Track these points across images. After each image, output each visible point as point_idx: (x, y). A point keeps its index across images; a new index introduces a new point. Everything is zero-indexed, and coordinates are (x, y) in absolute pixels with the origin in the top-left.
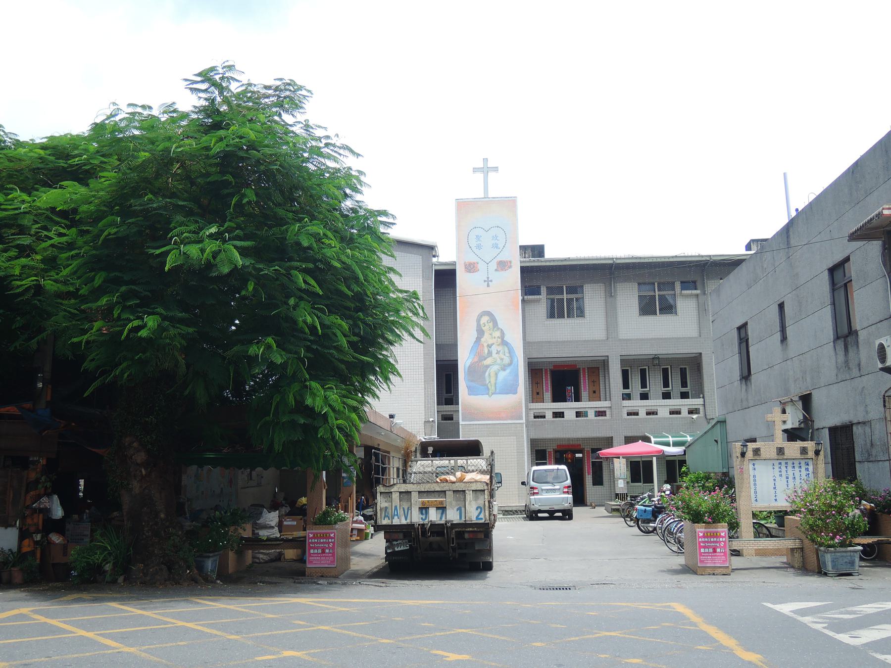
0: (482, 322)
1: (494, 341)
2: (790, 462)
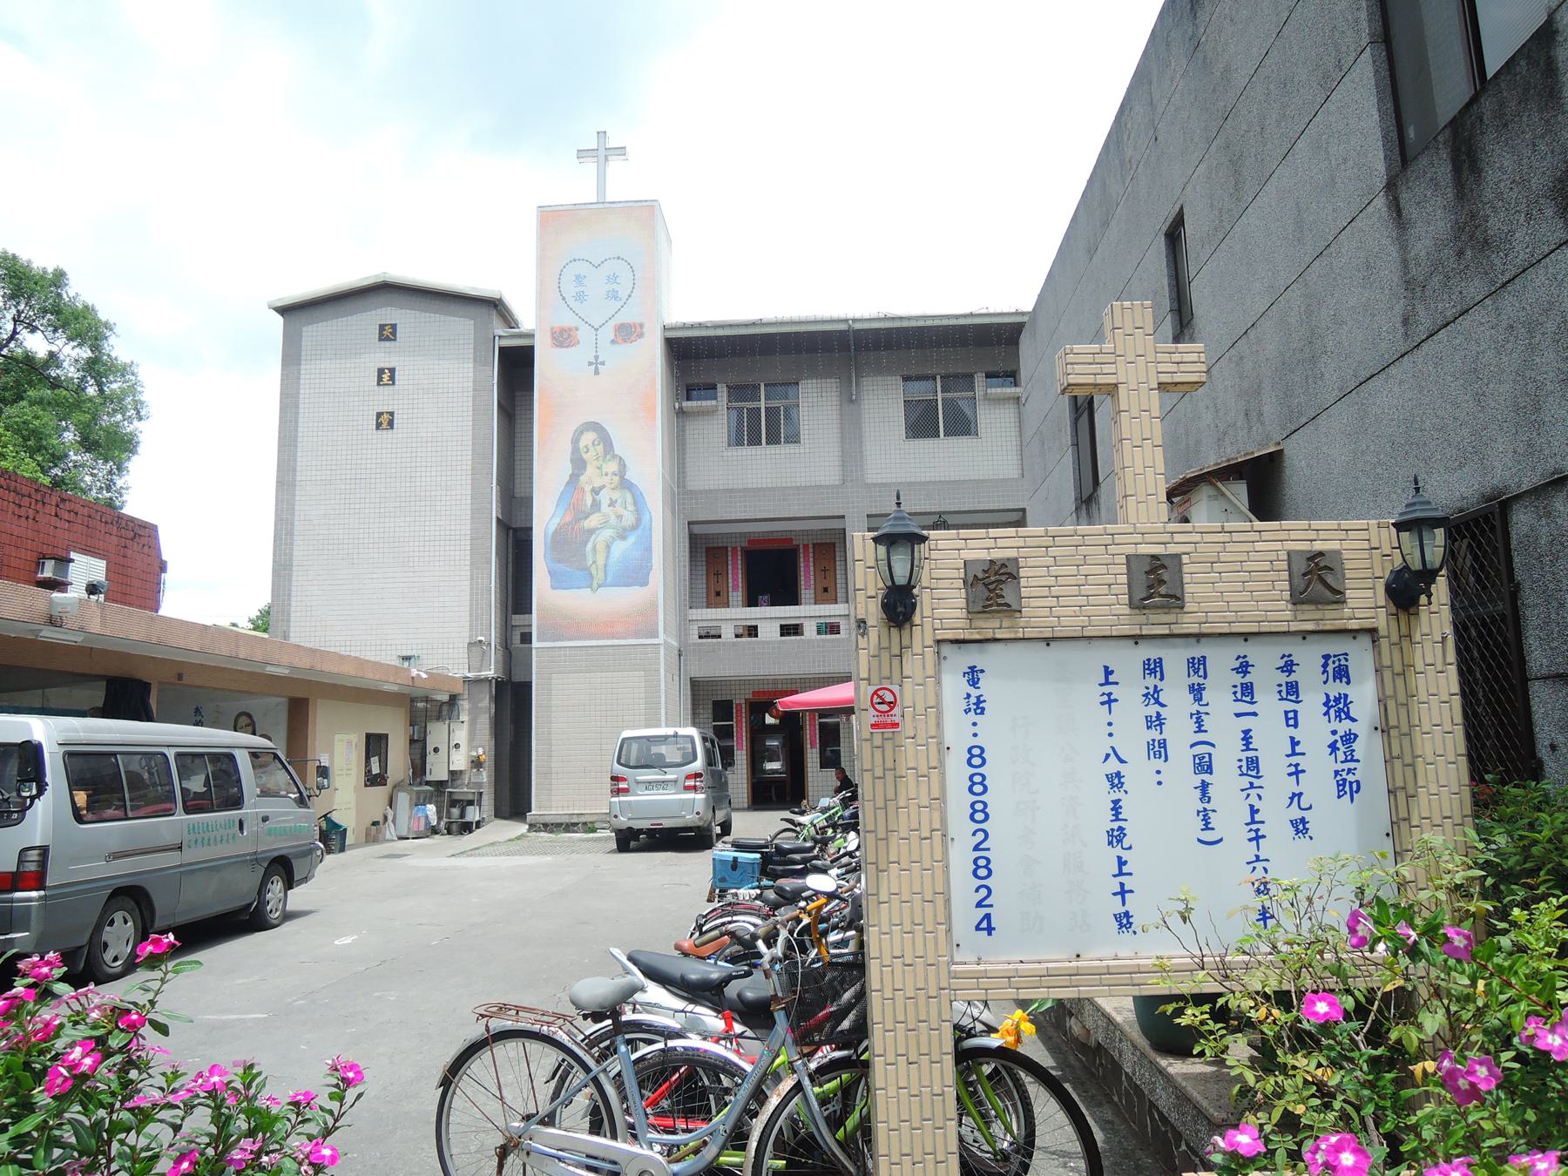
0: (582, 445)
1: (606, 480)
2: (1221, 660)
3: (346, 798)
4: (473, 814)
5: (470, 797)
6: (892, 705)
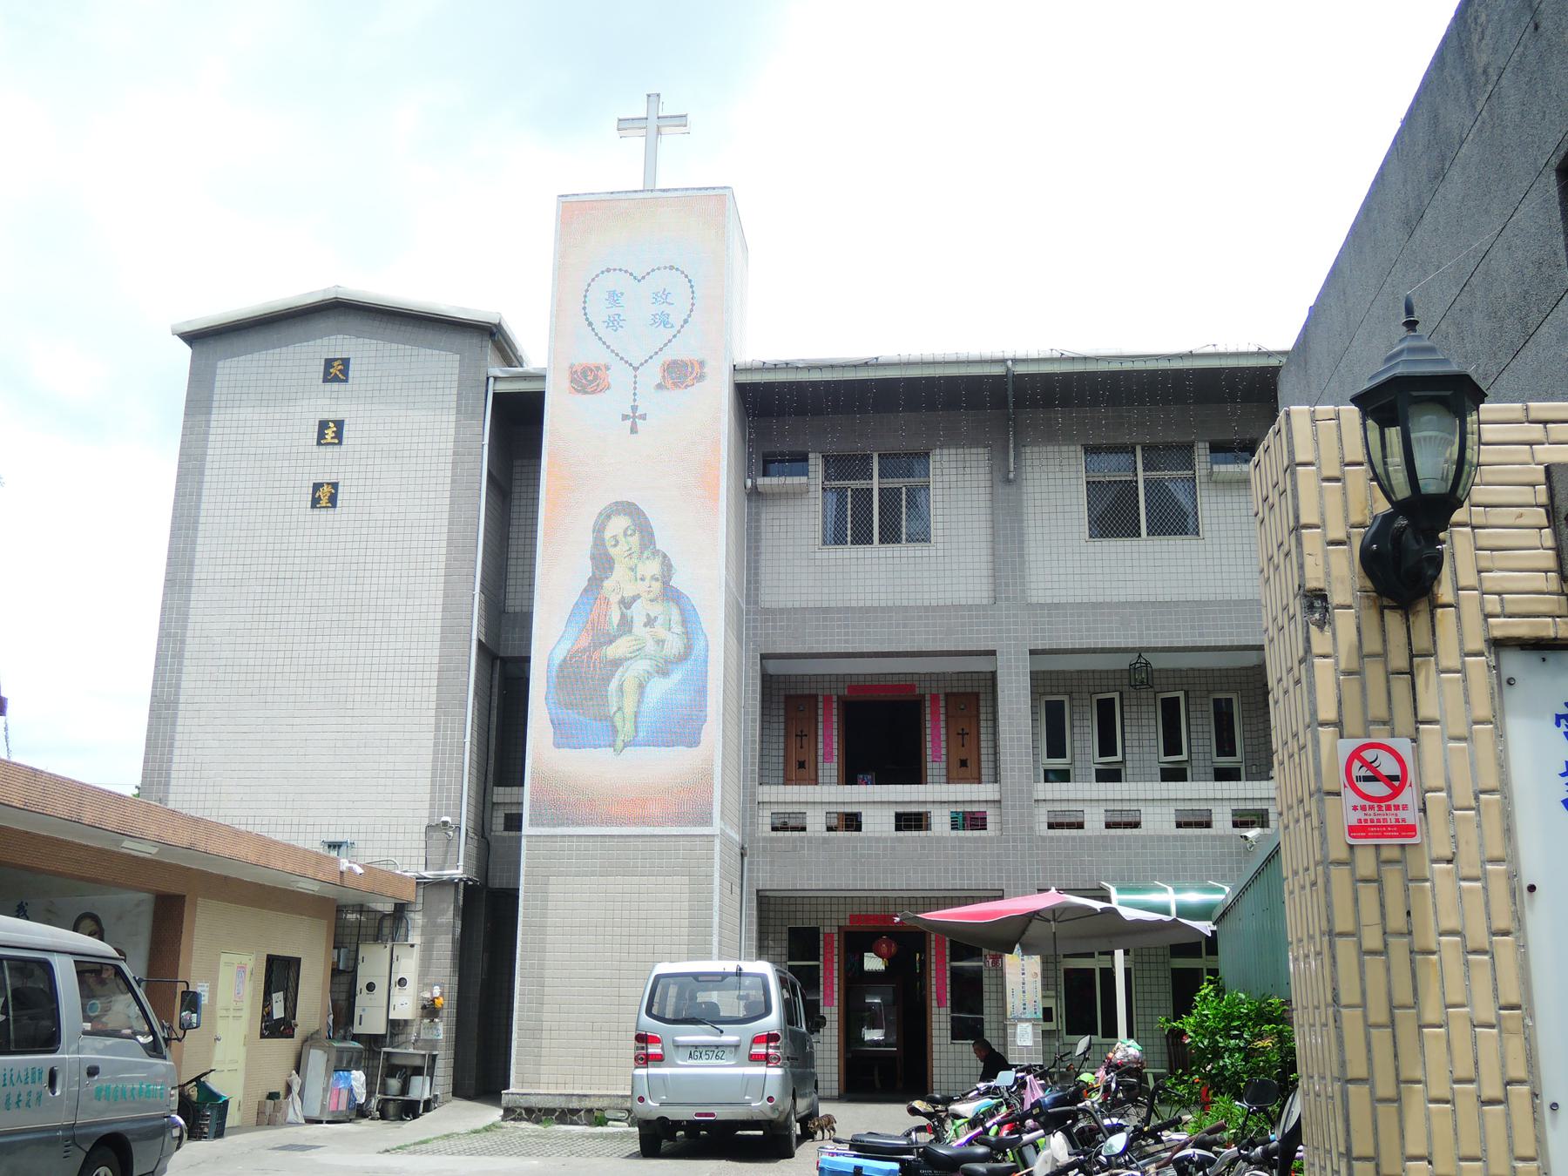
0: (608, 535)
1: (641, 587)
3: (229, 1049)
4: (420, 1089)
5: (418, 1062)
6: (1396, 783)
